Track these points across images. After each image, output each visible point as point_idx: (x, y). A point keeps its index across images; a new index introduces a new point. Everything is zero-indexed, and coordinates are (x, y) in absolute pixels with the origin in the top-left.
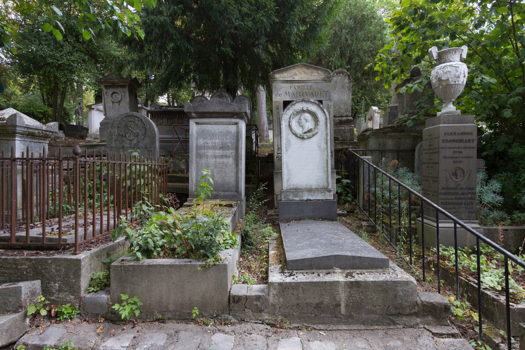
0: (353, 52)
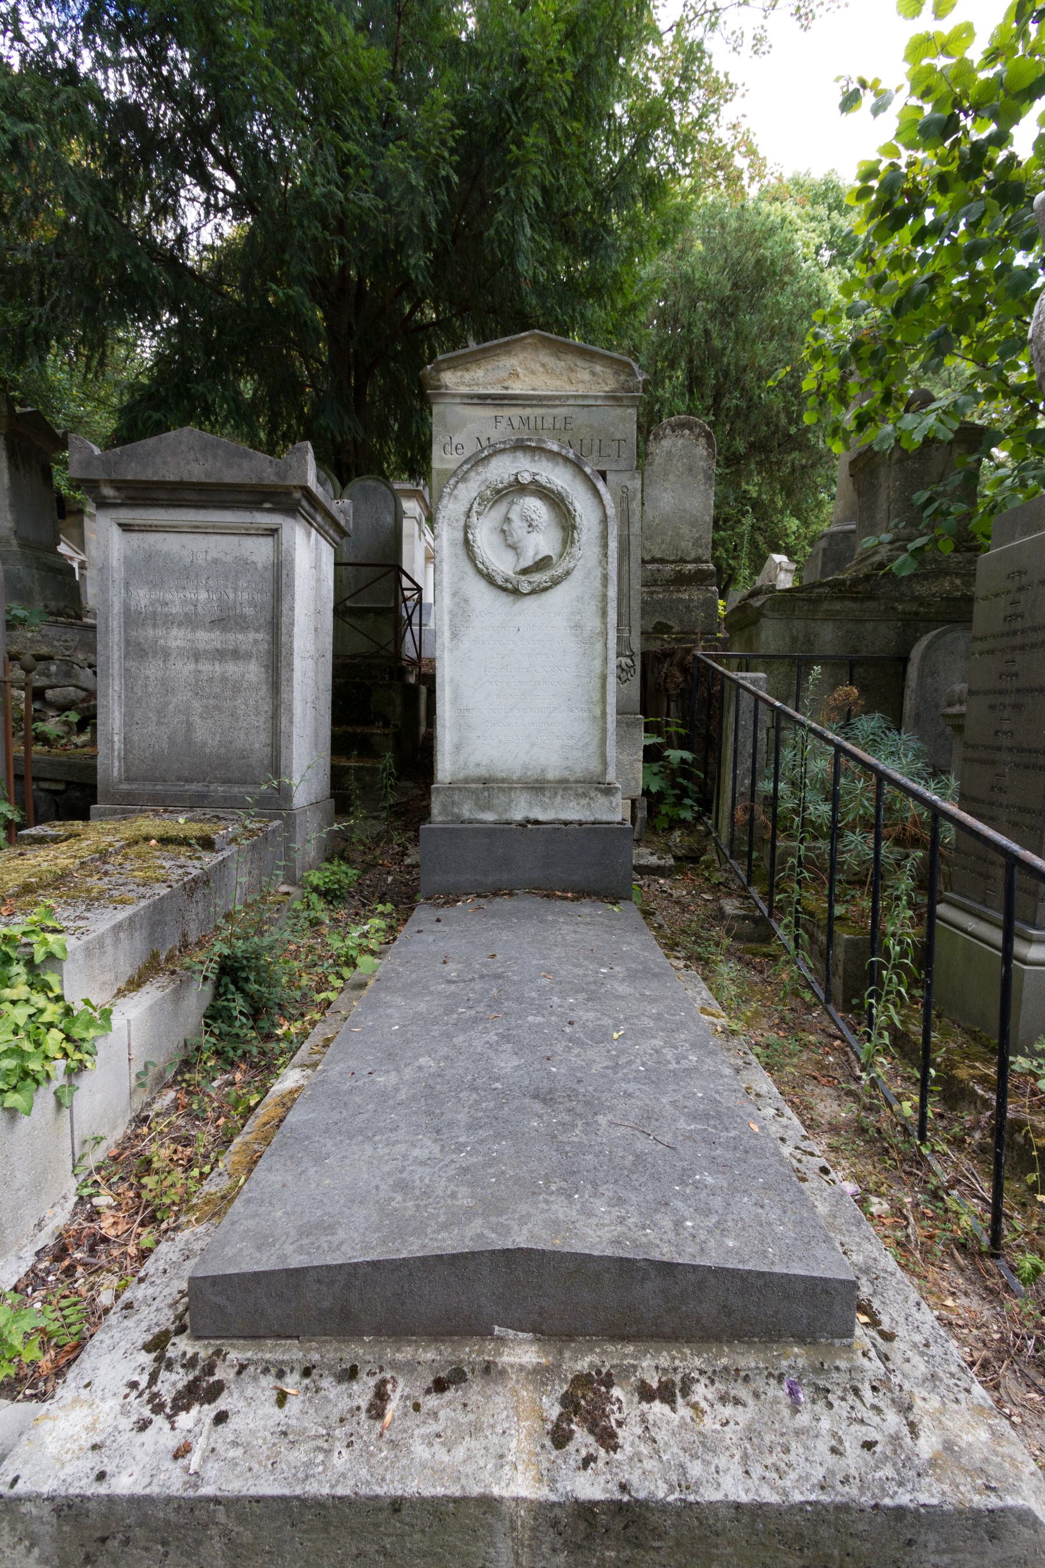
0: (726, 374)
